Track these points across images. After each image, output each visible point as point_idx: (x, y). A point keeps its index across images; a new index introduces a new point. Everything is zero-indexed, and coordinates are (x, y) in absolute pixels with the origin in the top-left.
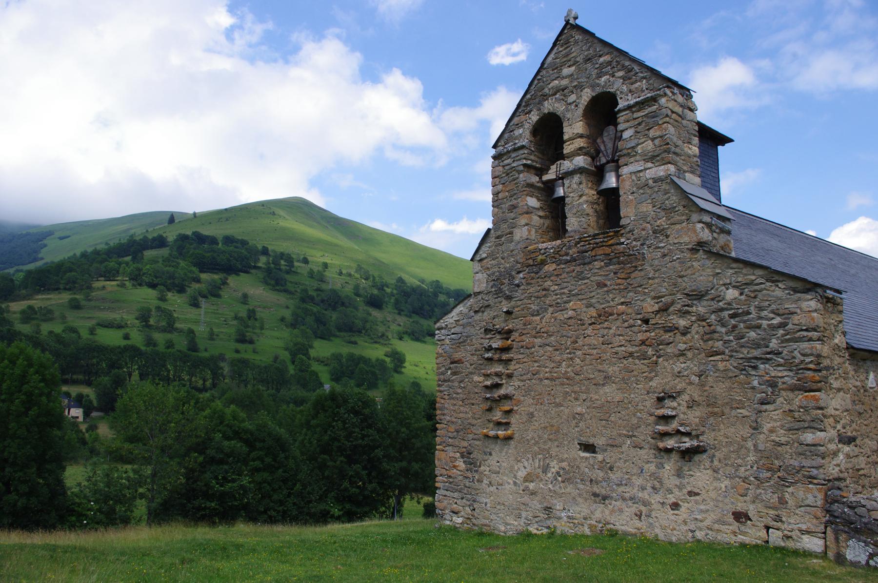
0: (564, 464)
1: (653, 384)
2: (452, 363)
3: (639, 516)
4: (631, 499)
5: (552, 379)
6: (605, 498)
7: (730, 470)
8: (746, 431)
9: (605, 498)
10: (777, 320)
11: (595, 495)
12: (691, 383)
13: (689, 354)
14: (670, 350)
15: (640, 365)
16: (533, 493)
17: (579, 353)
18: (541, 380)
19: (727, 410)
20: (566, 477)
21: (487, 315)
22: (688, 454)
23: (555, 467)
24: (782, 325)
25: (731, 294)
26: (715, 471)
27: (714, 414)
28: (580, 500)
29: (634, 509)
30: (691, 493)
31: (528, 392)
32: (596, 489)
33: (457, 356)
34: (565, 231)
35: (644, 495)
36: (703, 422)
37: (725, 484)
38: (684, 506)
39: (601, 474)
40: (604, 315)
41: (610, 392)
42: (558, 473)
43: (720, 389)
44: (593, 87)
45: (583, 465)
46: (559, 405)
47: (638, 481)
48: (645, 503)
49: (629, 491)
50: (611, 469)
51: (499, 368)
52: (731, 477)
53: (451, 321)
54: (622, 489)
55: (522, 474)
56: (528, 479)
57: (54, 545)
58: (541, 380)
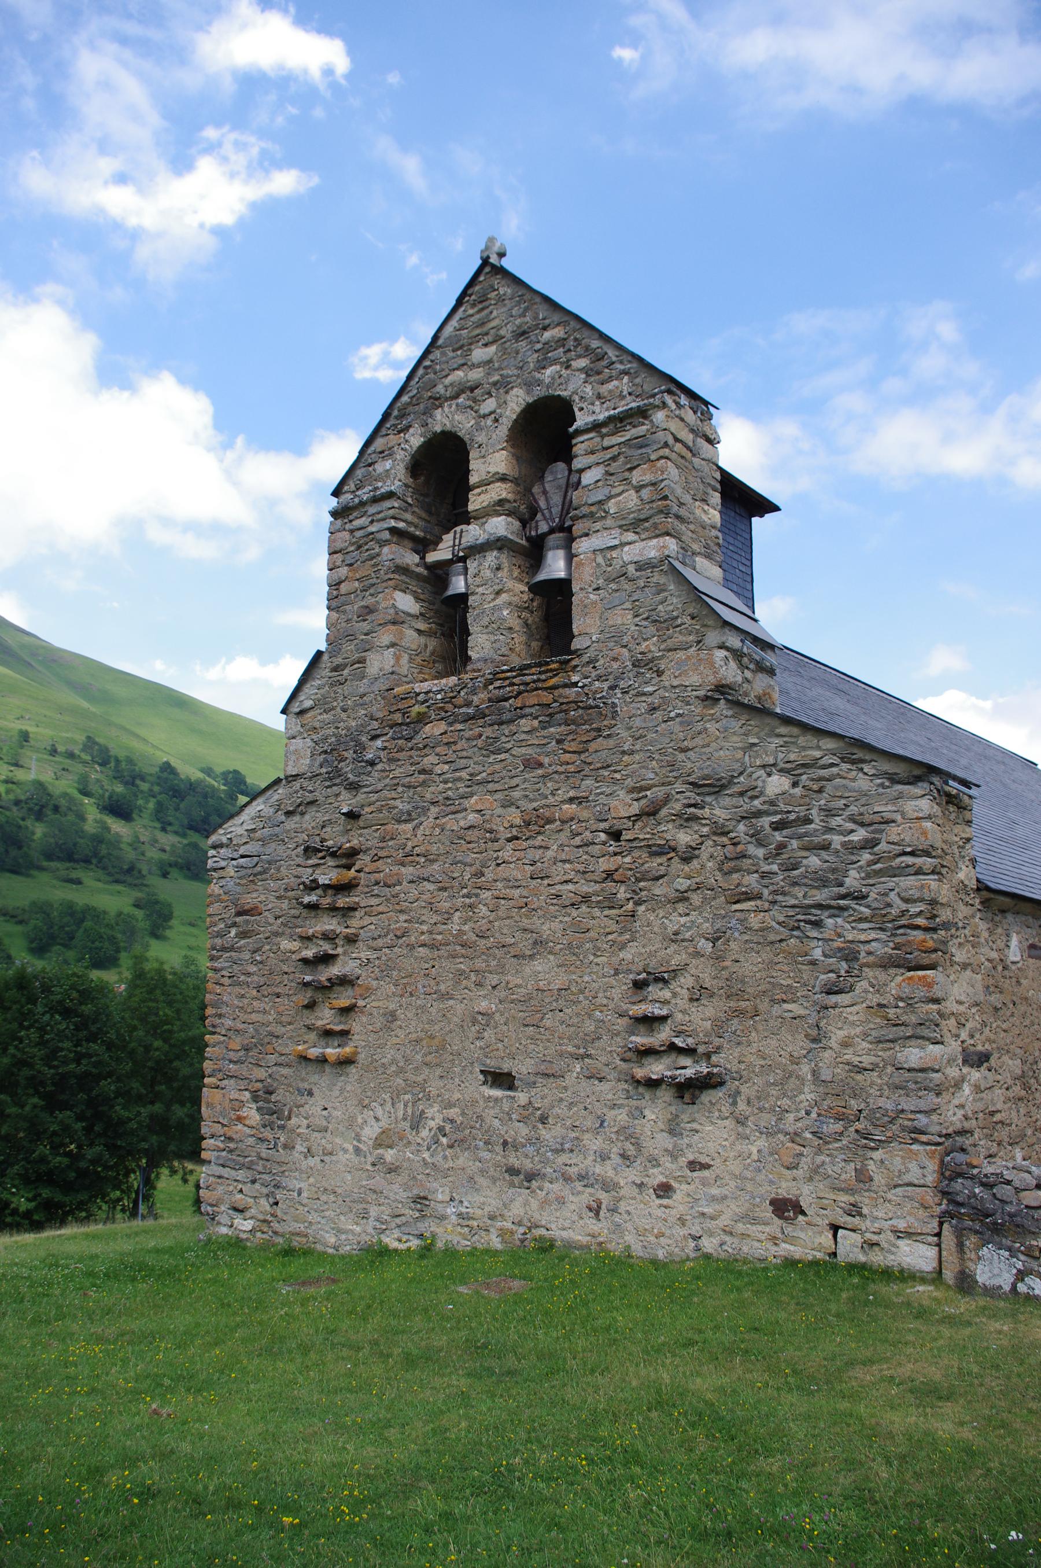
0: (453, 1112)
3: (595, 1210)
4: (581, 1177)
5: (433, 946)
6: (530, 1177)
7: (767, 1119)
8: (798, 1045)
9: (530, 1177)
10: (860, 835)
11: (513, 1171)
12: (697, 954)
13: (696, 898)
14: (659, 889)
17: (486, 895)
18: (411, 947)
20: (456, 1137)
21: (310, 820)
24: (870, 844)
25: (776, 784)
26: (741, 1121)
27: (739, 1013)
28: (483, 1182)
33: (249, 900)
35: (605, 1170)
36: (719, 1027)
38: (681, 1190)
39: (524, 1130)
40: (536, 823)
43: (751, 966)
47: (594, 1143)
48: (608, 1186)
49: (579, 1163)
50: (543, 1120)
51: (330, 924)
52: (769, 1133)
53: (240, 831)
54: (564, 1158)
55: (370, 1132)
56: (382, 1141)
58: (411, 947)
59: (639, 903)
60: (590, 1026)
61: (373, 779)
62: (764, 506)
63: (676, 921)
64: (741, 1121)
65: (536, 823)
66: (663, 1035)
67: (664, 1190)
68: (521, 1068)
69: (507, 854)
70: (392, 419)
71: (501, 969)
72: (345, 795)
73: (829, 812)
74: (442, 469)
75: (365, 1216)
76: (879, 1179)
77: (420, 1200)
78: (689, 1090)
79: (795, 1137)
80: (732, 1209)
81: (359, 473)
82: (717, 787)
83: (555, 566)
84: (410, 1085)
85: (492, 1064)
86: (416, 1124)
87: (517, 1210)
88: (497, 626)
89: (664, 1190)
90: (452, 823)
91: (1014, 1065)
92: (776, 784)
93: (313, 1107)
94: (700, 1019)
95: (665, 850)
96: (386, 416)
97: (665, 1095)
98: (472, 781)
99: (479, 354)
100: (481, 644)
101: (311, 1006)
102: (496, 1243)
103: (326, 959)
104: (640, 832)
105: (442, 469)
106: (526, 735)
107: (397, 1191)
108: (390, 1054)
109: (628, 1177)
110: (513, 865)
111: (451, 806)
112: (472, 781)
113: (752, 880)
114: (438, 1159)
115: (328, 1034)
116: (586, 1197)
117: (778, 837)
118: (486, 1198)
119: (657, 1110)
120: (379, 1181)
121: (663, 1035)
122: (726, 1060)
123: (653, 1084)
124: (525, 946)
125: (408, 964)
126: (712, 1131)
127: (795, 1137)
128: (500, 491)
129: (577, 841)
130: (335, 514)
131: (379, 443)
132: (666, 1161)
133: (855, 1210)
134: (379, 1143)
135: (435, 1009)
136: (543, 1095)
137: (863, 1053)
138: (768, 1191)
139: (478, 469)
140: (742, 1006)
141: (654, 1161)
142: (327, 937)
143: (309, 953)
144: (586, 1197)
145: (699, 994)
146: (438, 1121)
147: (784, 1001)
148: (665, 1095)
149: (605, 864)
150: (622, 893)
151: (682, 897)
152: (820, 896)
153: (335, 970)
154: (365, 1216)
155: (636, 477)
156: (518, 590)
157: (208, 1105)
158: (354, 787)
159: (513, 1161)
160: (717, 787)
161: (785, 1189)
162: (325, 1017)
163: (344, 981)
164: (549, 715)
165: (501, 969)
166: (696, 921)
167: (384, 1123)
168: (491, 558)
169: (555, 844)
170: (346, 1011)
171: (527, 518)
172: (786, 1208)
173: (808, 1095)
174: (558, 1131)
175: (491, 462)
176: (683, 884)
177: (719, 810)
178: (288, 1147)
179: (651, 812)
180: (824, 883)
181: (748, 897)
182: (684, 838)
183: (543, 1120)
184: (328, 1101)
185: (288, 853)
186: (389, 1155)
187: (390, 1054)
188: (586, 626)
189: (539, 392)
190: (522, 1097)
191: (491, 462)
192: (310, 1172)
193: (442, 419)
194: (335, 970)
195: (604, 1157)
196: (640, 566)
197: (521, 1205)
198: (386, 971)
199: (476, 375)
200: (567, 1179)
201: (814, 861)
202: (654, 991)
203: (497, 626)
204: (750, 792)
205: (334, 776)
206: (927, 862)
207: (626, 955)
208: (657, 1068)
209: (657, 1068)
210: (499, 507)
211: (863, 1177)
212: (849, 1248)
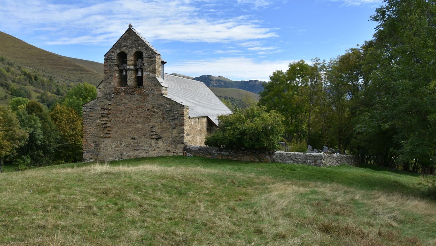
0: (126, 143)
6: (137, 150)
7: (166, 142)
8: (170, 134)
9: (137, 150)
11: (135, 149)
14: (154, 116)
18: (120, 122)
20: (127, 146)
24: (178, 113)
25: (168, 106)
36: (161, 132)
40: (138, 107)
43: (165, 125)
47: (146, 145)
48: (148, 150)
49: (143, 148)
55: (114, 146)
58: (120, 122)
61: (113, 99)
62: (165, 63)
63: (156, 120)
64: (163, 142)
65: (138, 107)
66: (154, 133)
67: (155, 150)
68: (136, 137)
69: (134, 111)
70: (115, 47)
71: (133, 125)
72: (108, 101)
73: (174, 109)
74: (123, 57)
75: (113, 157)
76: (178, 147)
77: (122, 154)
78: (158, 139)
79: (169, 143)
80: (163, 151)
81: (108, 54)
82: (161, 105)
83: (140, 74)
84: (120, 140)
85: (132, 137)
86: (121, 144)
87: (136, 154)
88: (131, 81)
89: (155, 150)
90: (125, 107)
91: (192, 135)
92: (168, 106)
93: (104, 143)
94: (159, 131)
95: (155, 112)
96: (113, 46)
97: (155, 140)
98: (129, 102)
99: (128, 41)
100: (129, 83)
101: (103, 130)
102: (133, 158)
103: (106, 124)
104: (152, 110)
105: (123, 57)
106: (136, 96)
107: (118, 153)
111: (125, 104)
112: (129, 102)
113: (165, 116)
115: (106, 134)
116: (145, 152)
118: (132, 153)
119: (153, 142)
120: (115, 152)
121: (154, 133)
122: (162, 136)
123: (153, 139)
124: (136, 122)
126: (160, 143)
127: (169, 143)
128: (132, 62)
130: (105, 60)
131: (112, 50)
133: (175, 151)
134: (115, 147)
135: (123, 130)
136: (139, 140)
138: (166, 149)
139: (129, 58)
140: (164, 130)
141: (153, 147)
142: (106, 121)
143: (103, 123)
144: (145, 152)
145: (158, 129)
147: (58, 31)
148: (155, 140)
149: (147, 113)
150: (149, 117)
151: (157, 118)
152: (172, 118)
153: (107, 125)
154: (113, 157)
155: (152, 65)
156: (134, 76)
158: (110, 100)
159: (135, 148)
160: (161, 105)
161: (168, 149)
162: (106, 131)
163: (109, 127)
164: (140, 94)
165: (133, 125)
166: (158, 120)
167: (116, 145)
168: (131, 71)
169: (140, 110)
170: (109, 131)
171: (135, 65)
172: (168, 151)
173: (171, 139)
175: (131, 58)
176: (157, 116)
177: (161, 108)
178: (100, 149)
179: (153, 107)
180: (173, 117)
182: (157, 111)
184: (107, 142)
185: (99, 109)
186: (117, 149)
187: (116, 136)
188: (145, 84)
189: (138, 50)
190: (136, 141)
191: (131, 58)
192: (104, 152)
193: (123, 49)
194: (107, 125)
195: (147, 147)
196: (152, 77)
197: (136, 153)
198: (116, 125)
199: (128, 44)
200: (142, 150)
201: (172, 115)
202: (154, 128)
203: (131, 81)
204: (165, 106)
205: (106, 98)
207: (150, 124)
208: (154, 137)
209: (154, 137)
210: (132, 65)
211: (176, 147)
212: (175, 154)
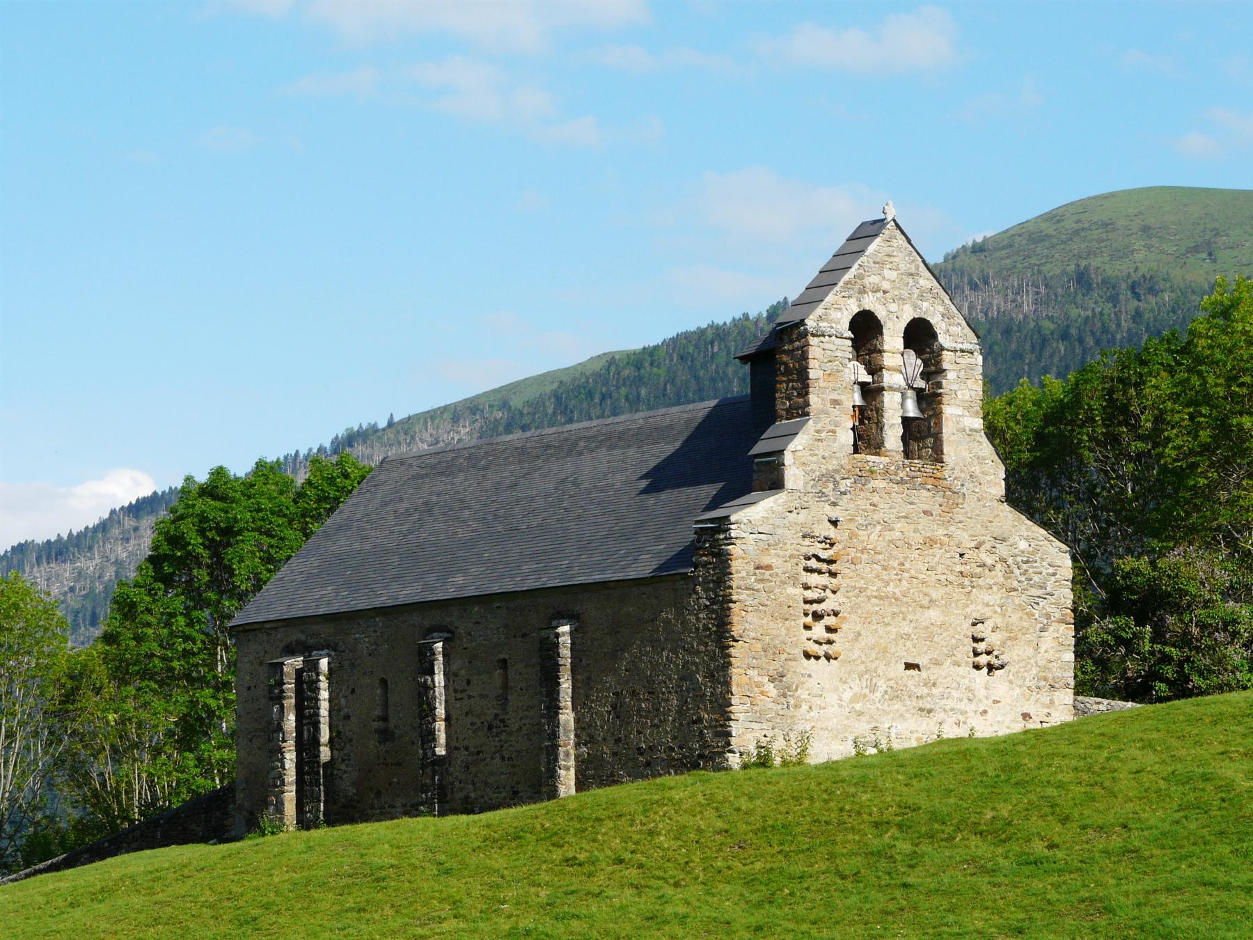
0: (892, 683)
1: (969, 610)
2: (758, 568)
3: (958, 724)
4: (952, 710)
5: (881, 598)
6: (930, 711)
7: (1020, 682)
8: (1030, 651)
9: (930, 711)
10: (1051, 570)
11: (921, 710)
12: (996, 612)
13: (995, 588)
14: (981, 582)
15: (957, 593)
16: (860, 714)
17: (906, 575)
18: (869, 598)
19: (1019, 635)
20: (895, 694)
21: (803, 516)
22: (991, 668)
23: (882, 685)
24: (1054, 574)
25: (1023, 545)
26: (1011, 682)
27: (1010, 638)
28: (907, 715)
29: (953, 720)
30: (996, 702)
31: (854, 609)
32: (921, 704)
33: (765, 561)
34: (1040, 476)
35: (961, 706)
36: (1003, 644)
37: (1018, 691)
38: (990, 713)
39: (926, 691)
40: (930, 542)
41: (933, 614)
42: (886, 692)
43: (1014, 618)
44: (915, 307)
45: (910, 683)
46: (888, 624)
47: (955, 694)
48: (964, 713)
49: (950, 704)
50: (934, 685)
51: (824, 580)
52: (1020, 687)
53: (757, 517)
54: (944, 701)
55: (847, 695)
56: (857, 698)
57: (1078, 655)
58: (869, 598)
59: (973, 587)
60: (954, 641)
108: (857, 653)
109: (970, 708)
110: (917, 565)
113: (1015, 584)
114: (885, 707)
117: (1025, 566)
124: (925, 602)
125: (869, 607)
129: (948, 555)
132: (986, 702)
137: (1050, 656)
146: (884, 688)
150: (966, 581)
157: (738, 685)
172: (1026, 716)
174: (941, 689)
177: (1002, 550)
181: (1015, 590)
183: (934, 685)
195: (961, 700)
206: (813, 563)
